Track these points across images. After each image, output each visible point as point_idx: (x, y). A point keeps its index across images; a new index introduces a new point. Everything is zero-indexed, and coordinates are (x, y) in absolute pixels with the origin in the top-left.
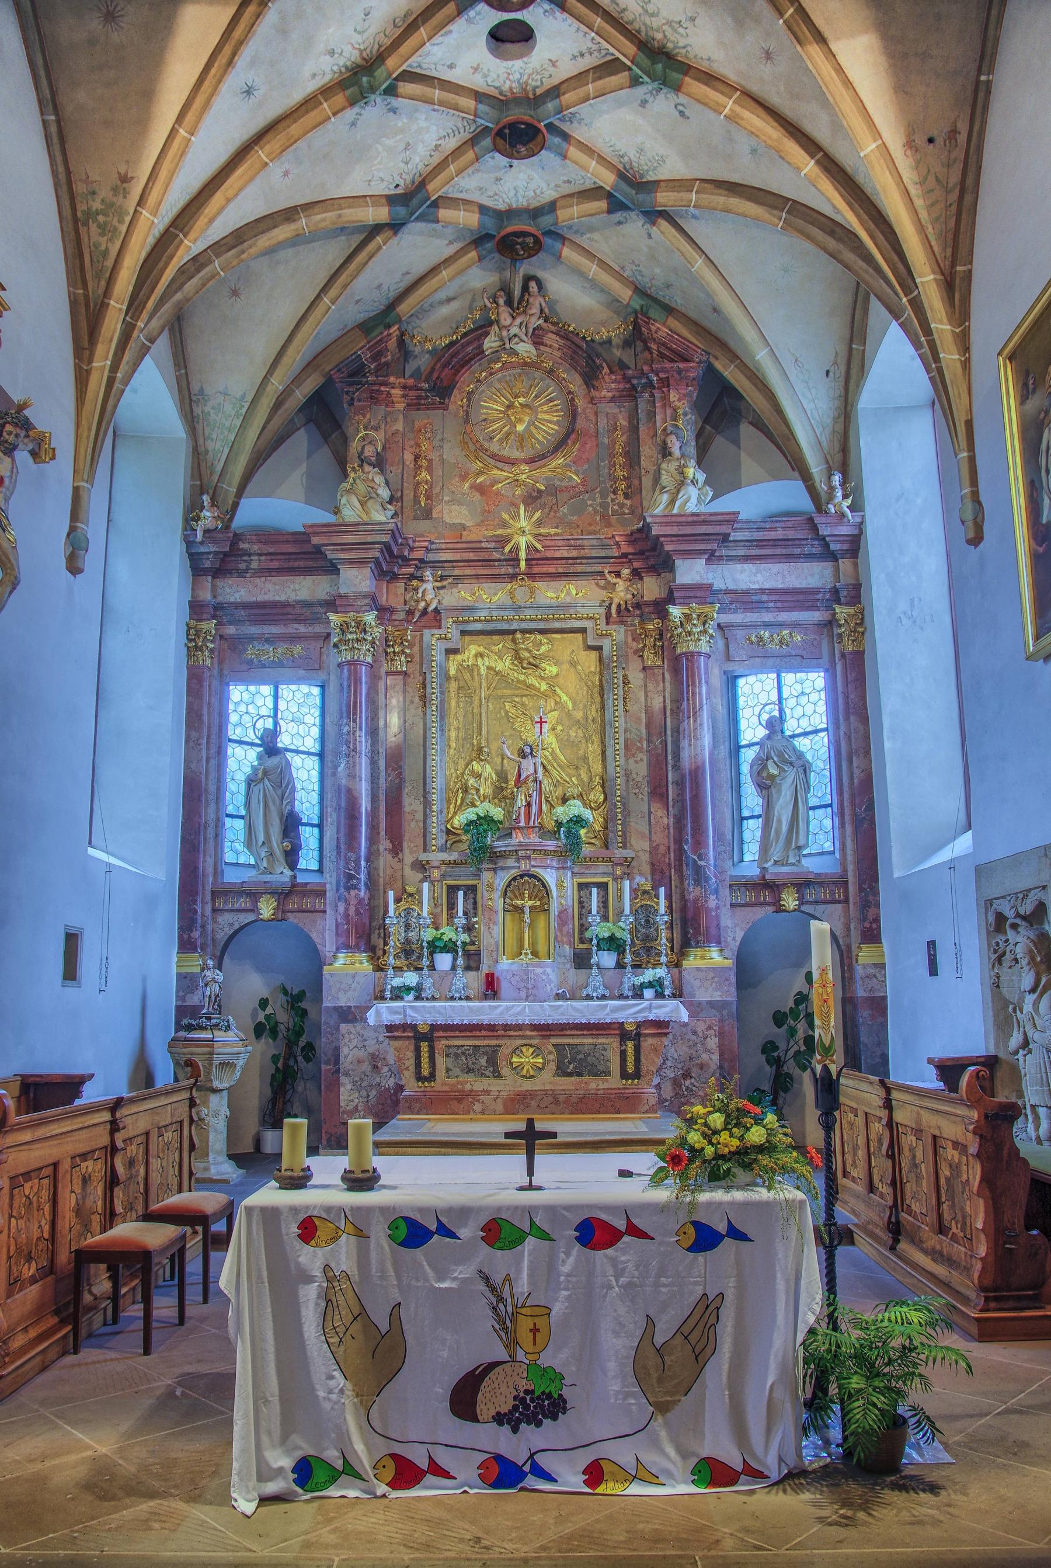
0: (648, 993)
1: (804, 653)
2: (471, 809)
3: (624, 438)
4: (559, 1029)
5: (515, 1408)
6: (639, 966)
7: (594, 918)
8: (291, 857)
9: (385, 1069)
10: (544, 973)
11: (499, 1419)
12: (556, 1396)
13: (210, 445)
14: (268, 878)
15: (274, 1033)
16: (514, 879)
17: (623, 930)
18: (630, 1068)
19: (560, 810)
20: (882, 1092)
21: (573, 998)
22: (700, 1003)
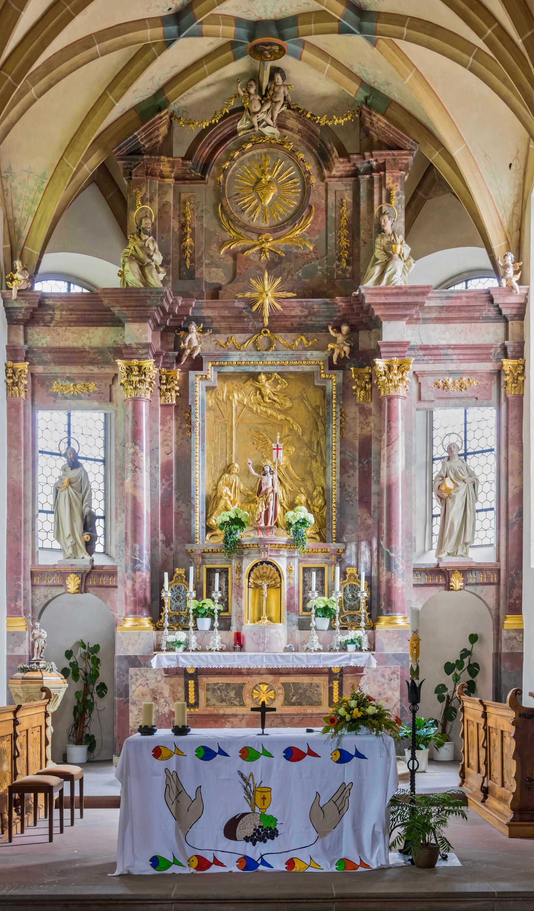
0: (351, 647)
1: (478, 395)
2: (224, 513)
3: (349, 212)
4: (288, 672)
5: (254, 834)
6: (346, 629)
7: (314, 594)
8: (89, 546)
9: (162, 700)
10: (276, 633)
11: (247, 839)
12: (273, 829)
13: (18, 214)
14: (73, 561)
15: (76, 676)
16: (256, 565)
17: (334, 602)
18: (192, 700)
19: (290, 514)
20: (481, 708)
21: (297, 650)
22: (387, 656)
